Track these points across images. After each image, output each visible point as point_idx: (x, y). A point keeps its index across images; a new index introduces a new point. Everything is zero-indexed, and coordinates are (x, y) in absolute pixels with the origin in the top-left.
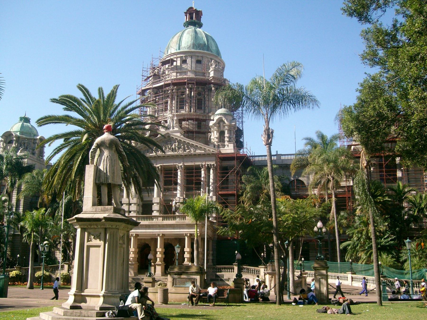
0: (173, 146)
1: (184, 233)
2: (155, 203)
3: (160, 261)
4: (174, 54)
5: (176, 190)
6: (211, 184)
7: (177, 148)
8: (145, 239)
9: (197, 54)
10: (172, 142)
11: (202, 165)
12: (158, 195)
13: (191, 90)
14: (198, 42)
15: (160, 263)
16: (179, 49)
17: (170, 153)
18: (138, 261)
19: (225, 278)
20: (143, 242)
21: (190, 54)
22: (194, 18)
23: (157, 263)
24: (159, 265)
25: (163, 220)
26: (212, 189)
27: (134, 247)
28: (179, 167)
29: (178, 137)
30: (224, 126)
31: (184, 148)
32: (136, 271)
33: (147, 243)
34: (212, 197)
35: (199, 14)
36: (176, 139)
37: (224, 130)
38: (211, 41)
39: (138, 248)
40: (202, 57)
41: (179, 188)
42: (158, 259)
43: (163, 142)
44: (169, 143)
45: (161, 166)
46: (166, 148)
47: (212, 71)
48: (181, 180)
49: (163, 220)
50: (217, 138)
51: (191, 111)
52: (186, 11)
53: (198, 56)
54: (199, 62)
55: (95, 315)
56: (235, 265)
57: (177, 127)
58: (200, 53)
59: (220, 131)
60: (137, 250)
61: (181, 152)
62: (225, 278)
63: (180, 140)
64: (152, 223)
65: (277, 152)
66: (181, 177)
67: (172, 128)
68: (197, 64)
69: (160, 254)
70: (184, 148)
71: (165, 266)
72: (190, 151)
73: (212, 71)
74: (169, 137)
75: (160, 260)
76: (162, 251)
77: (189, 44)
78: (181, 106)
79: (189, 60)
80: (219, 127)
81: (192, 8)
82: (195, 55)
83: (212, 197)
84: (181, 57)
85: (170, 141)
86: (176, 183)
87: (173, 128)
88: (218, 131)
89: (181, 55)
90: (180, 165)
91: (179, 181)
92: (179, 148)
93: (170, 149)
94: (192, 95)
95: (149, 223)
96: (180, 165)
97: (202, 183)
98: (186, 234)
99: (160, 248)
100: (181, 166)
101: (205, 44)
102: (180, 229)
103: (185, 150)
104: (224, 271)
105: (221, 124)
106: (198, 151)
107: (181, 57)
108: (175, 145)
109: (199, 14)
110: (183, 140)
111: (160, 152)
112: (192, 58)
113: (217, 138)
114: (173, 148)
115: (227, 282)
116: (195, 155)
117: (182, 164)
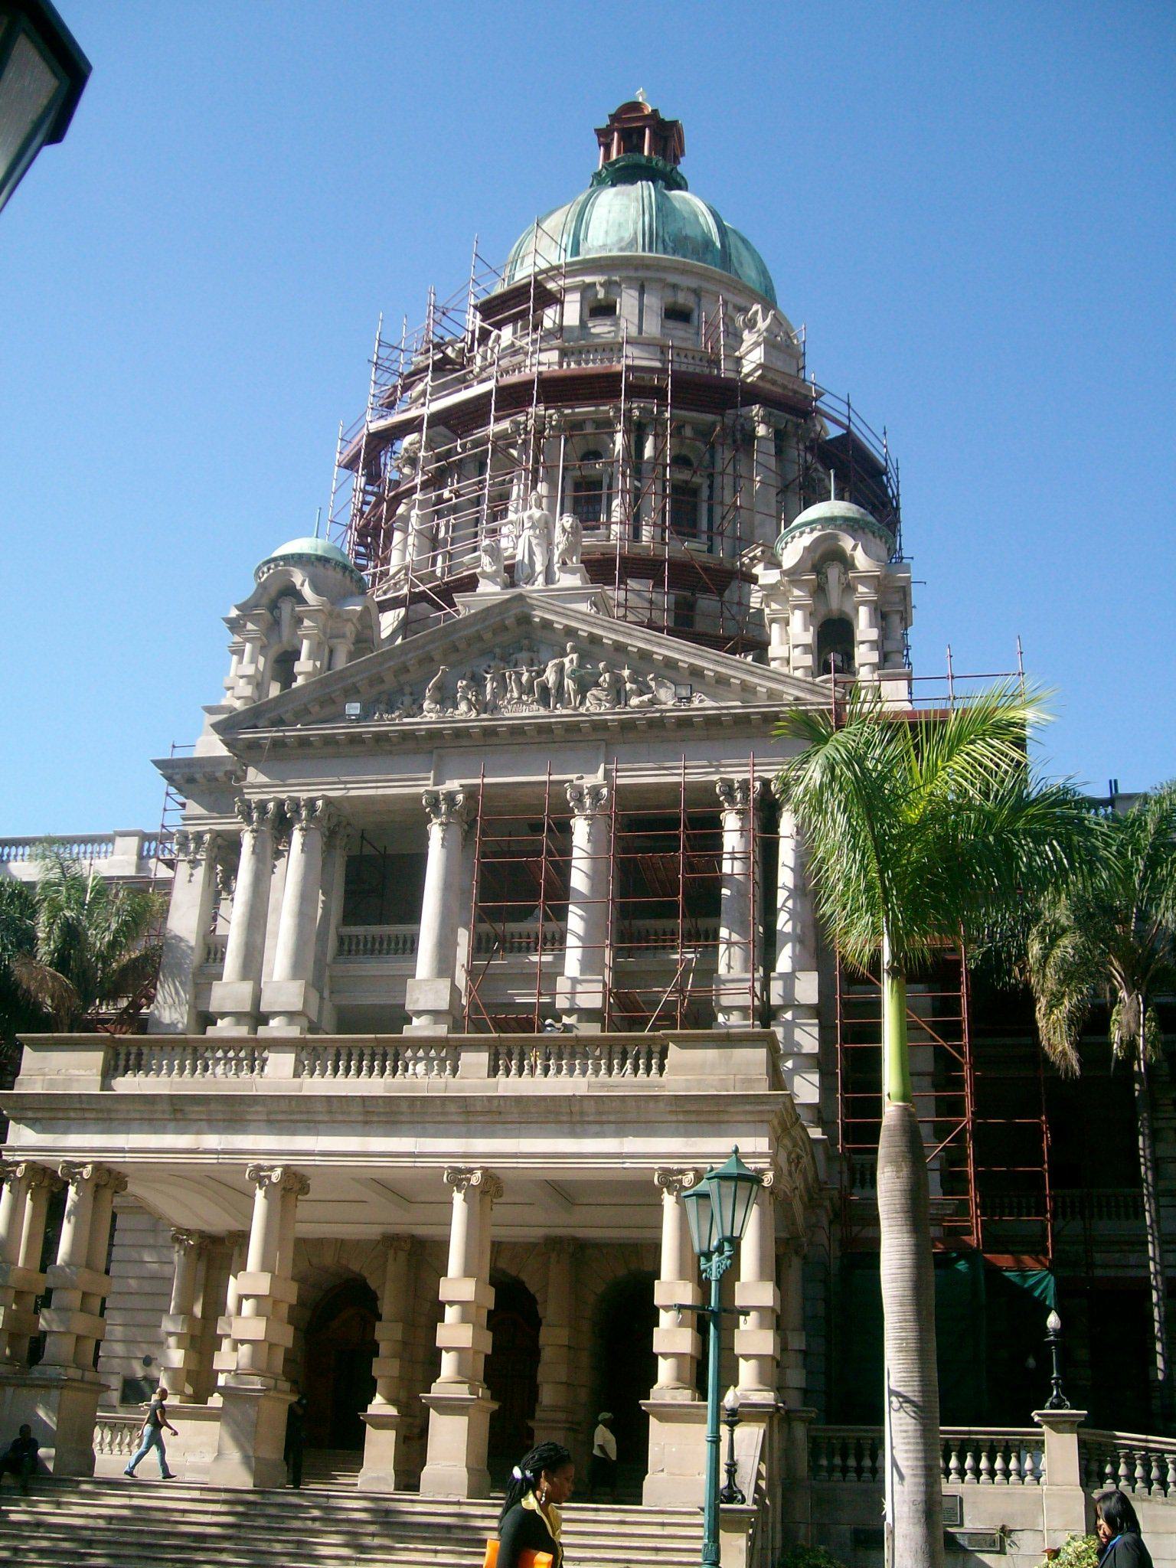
0: (550, 676)
1: (657, 1164)
2: (420, 1013)
3: (463, 1375)
4: (554, 271)
5: (557, 942)
6: (782, 895)
7: (569, 684)
8: (341, 1244)
9: (673, 278)
10: (543, 656)
11: (728, 785)
12: (444, 966)
13: (637, 432)
14: (672, 228)
15: (462, 1392)
16: (576, 251)
17: (530, 711)
18: (287, 1374)
19: (971, 1524)
20: (328, 1259)
21: (632, 274)
22: (643, 147)
23: (438, 1390)
24: (449, 1407)
25: (493, 1071)
26: (788, 928)
27: (265, 1266)
28: (579, 799)
29: (583, 618)
30: (849, 588)
31: (617, 684)
32: (273, 1450)
33: (355, 1267)
34: (789, 979)
35: (668, 135)
36: (570, 632)
37: (848, 609)
38: (732, 239)
39: (300, 1278)
40: (697, 293)
41: (575, 921)
42: (448, 1364)
43: (483, 653)
44: (524, 655)
45: (471, 792)
46: (503, 686)
47: (757, 344)
48: (593, 877)
49: (493, 1071)
50: (806, 648)
51: (636, 534)
52: (604, 123)
53: (675, 287)
54: (676, 314)
55: (503, 1234)
56: (1057, 1425)
57: (573, 572)
58: (684, 270)
59: (822, 611)
60: (291, 1293)
61: (596, 705)
62: (971, 1524)
63: (594, 639)
64: (413, 1087)
65: (1114, 784)
66: (593, 858)
67: (541, 579)
68: (671, 324)
69: (464, 1319)
70: (617, 684)
71: (494, 1417)
72: (653, 702)
73: (757, 344)
74: (525, 620)
75: (460, 1370)
76: (476, 1304)
77: (627, 235)
78: (586, 500)
79: (627, 302)
80: (819, 591)
81: (636, 106)
82: (660, 280)
83: (789, 979)
84: (586, 289)
85: (530, 649)
86: (560, 892)
87: (549, 579)
88: (811, 615)
89: (588, 279)
90: (589, 781)
91: (579, 881)
92: (582, 690)
93: (530, 691)
94: (648, 452)
95: (387, 1088)
96: (589, 781)
97: (725, 891)
98: (666, 1172)
99: (467, 1273)
100: (595, 791)
101: (708, 243)
102: (620, 1134)
103: (618, 695)
104: (962, 1473)
105: (833, 573)
106: (703, 703)
107: (586, 289)
108: (560, 669)
109: (668, 135)
110: (609, 637)
111: (463, 707)
112: (642, 291)
113: (806, 648)
114: (544, 688)
115: (986, 1558)
116: (684, 723)
117: (597, 778)
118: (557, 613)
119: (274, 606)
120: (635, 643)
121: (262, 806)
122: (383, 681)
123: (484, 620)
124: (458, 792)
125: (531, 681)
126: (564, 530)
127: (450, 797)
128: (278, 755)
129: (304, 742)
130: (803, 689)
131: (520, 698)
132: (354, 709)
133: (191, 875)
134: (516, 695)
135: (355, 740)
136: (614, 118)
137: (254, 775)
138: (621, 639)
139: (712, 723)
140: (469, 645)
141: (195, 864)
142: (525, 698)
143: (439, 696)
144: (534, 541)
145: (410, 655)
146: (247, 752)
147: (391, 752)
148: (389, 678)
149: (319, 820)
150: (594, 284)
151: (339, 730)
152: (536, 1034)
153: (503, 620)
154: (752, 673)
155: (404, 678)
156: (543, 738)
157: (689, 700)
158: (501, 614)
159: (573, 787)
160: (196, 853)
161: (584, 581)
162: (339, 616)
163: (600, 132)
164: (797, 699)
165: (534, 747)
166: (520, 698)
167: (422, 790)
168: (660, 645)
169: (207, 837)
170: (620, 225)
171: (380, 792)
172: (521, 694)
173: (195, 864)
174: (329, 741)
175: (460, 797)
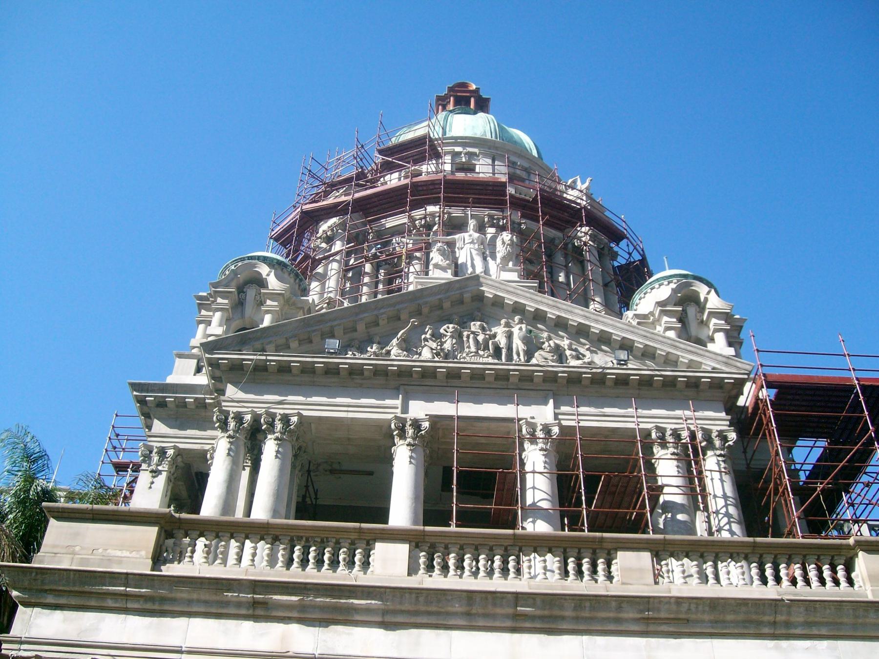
30: (703, 324)
45: (435, 420)
53: (514, 163)
93: (486, 348)
118: (508, 292)
119: (241, 290)
120: (575, 319)
121: (239, 418)
122: (356, 330)
123: (447, 291)
124: (423, 420)
125: (486, 342)
126: (504, 243)
127: (416, 424)
128: (258, 377)
129: (284, 369)
130: (719, 362)
131: (477, 352)
132: (333, 344)
133: (152, 483)
134: (473, 349)
135: (332, 371)
136: (451, 89)
137: (231, 391)
138: (563, 315)
139: (646, 382)
140: (431, 311)
141: (156, 473)
142: (481, 353)
143: (404, 346)
144: (473, 251)
145: (382, 311)
146: (224, 373)
147: (361, 386)
148: (361, 327)
149: (290, 431)
150: (460, 153)
151: (320, 361)
152: (770, 539)
153: (462, 294)
154: (676, 347)
155: (374, 330)
156: (500, 384)
157: (626, 362)
158: (460, 288)
159: (528, 423)
160: (158, 465)
161: (520, 276)
162: (294, 304)
163: (439, 98)
164: (714, 368)
165: (491, 391)
166: (477, 352)
167: (390, 416)
168: (596, 321)
169: (171, 452)
170: (473, 127)
171: (351, 415)
172: (478, 349)
173: (156, 473)
174: (308, 370)
175: (426, 425)
